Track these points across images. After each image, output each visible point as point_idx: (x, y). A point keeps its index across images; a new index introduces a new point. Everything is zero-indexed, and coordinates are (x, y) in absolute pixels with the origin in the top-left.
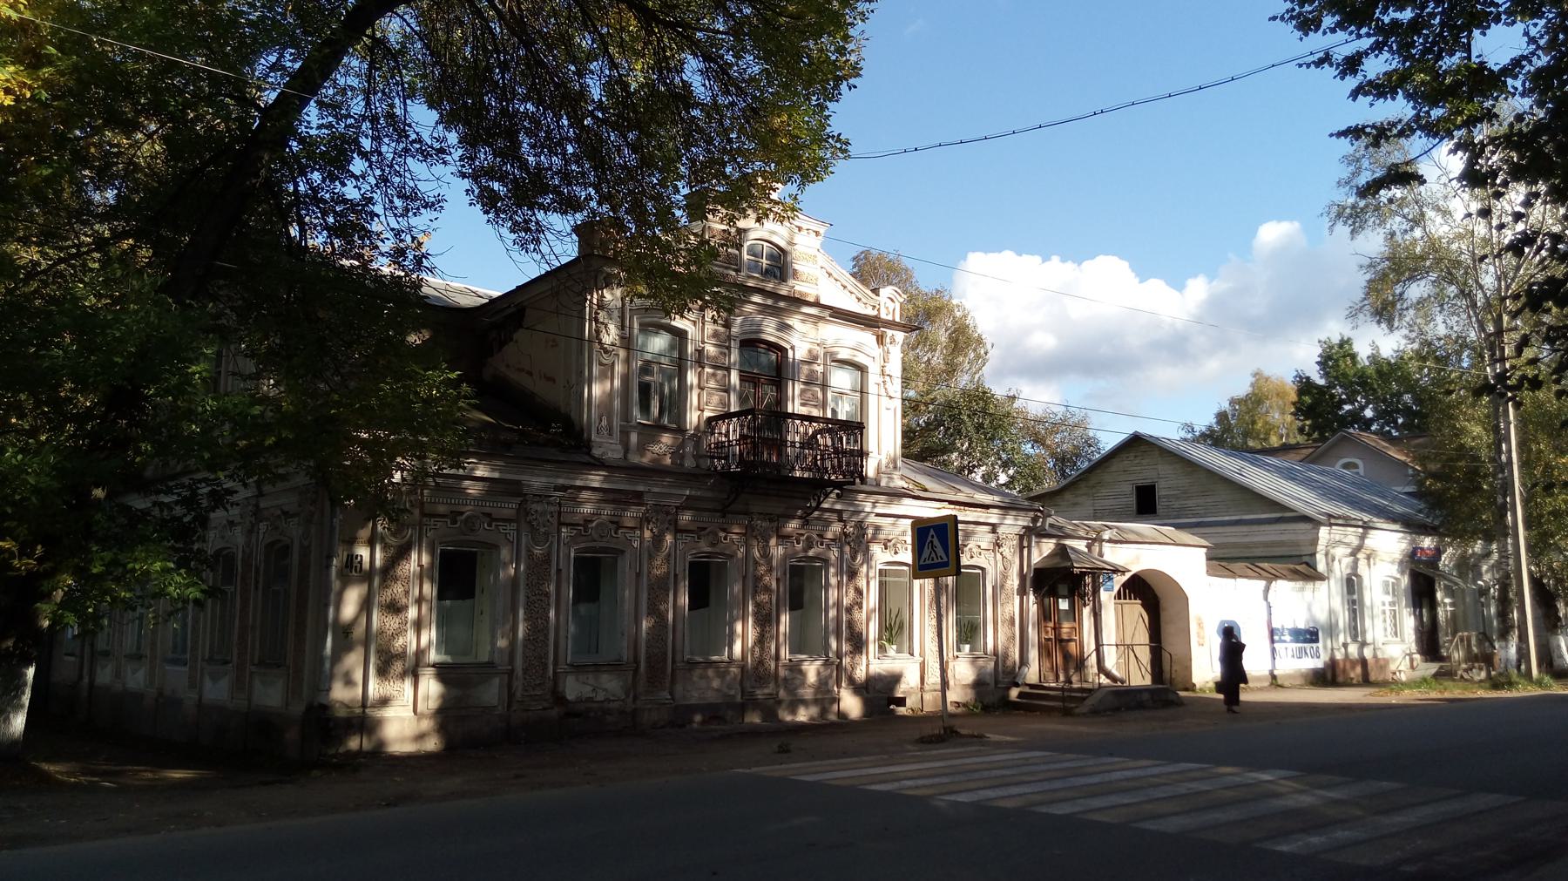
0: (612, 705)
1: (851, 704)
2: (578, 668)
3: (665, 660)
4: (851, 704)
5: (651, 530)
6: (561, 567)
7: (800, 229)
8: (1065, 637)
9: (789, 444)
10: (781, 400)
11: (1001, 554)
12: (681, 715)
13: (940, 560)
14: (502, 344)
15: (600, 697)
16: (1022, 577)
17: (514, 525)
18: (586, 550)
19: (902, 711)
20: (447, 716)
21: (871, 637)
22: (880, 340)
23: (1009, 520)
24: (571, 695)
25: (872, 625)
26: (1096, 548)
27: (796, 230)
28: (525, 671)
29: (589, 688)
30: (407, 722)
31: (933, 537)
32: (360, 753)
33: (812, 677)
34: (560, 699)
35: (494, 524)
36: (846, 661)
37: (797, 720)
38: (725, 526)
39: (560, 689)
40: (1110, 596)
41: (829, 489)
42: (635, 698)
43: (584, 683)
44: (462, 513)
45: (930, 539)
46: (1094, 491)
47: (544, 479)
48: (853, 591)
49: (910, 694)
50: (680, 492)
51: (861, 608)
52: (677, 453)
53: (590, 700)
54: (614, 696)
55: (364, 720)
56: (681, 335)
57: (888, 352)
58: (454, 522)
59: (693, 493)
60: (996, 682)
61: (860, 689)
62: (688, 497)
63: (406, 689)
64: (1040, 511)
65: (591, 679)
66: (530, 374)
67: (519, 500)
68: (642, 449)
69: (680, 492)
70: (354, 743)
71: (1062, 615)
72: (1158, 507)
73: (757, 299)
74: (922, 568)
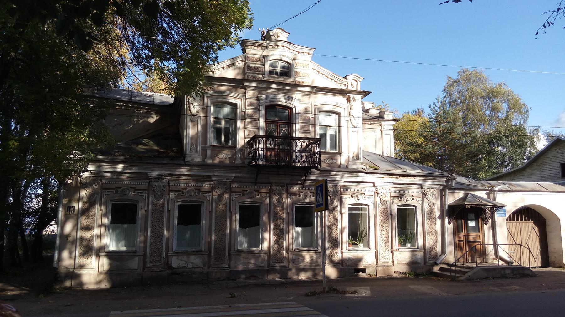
0: (196, 270)
1: (331, 272)
2: (178, 253)
3: (224, 250)
4: (331, 272)
5: (217, 192)
7: (299, 53)
8: (471, 240)
10: (290, 131)
11: (427, 198)
12: (233, 275)
15: (190, 266)
16: (442, 210)
17: (146, 192)
18: (183, 202)
19: (361, 275)
20: (110, 273)
21: (344, 240)
22: (348, 100)
23: (429, 182)
25: (344, 234)
26: (492, 195)
27: (297, 53)
28: (151, 255)
29: (184, 262)
30: (92, 275)
32: (70, 288)
33: (308, 259)
34: (170, 267)
36: (328, 252)
37: (300, 278)
38: (257, 189)
39: (169, 263)
40: (504, 220)
42: (209, 267)
44: (121, 187)
46: (541, 167)
47: (158, 172)
48: (332, 218)
49: (369, 267)
50: (230, 175)
51: (337, 226)
52: (233, 158)
54: (197, 266)
55: (73, 275)
56: (234, 106)
57: (352, 105)
58: (117, 191)
59: (237, 175)
60: (425, 262)
61: (335, 265)
62: (235, 177)
63: (93, 261)
64: (449, 177)
65: (185, 258)
67: (148, 181)
68: (213, 157)
69: (230, 175)
70: (68, 284)
71: (469, 229)
73: (273, 86)
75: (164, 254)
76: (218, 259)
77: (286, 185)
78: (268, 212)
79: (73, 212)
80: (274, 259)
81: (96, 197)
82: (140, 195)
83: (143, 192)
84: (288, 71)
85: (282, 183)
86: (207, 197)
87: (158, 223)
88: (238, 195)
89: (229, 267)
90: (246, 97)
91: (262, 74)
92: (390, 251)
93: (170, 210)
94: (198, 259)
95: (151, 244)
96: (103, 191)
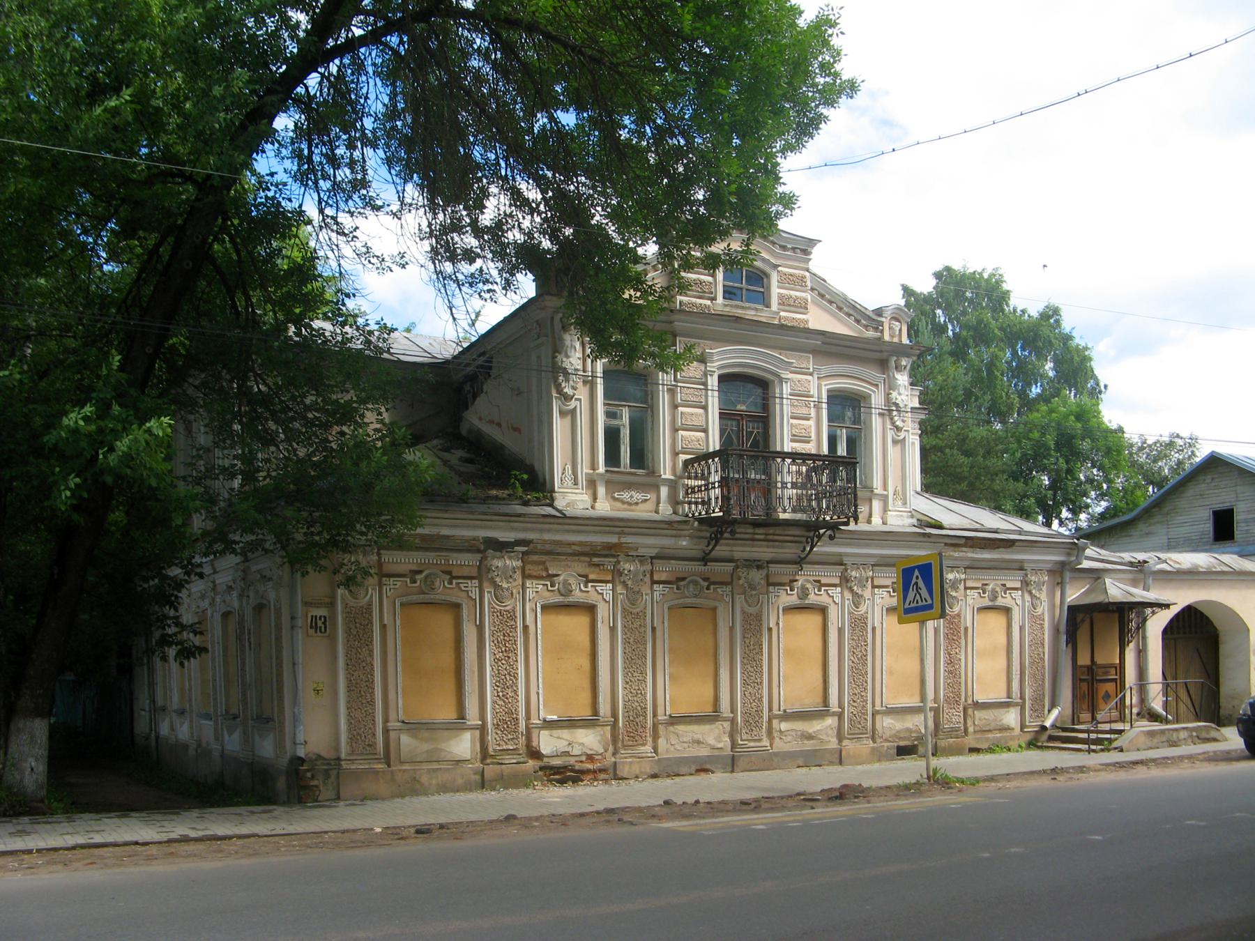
2: (549, 725)
9: (779, 485)
13: (924, 603)
14: (475, 396)
17: (476, 582)
24: (545, 750)
28: (497, 726)
31: (917, 578)
35: (454, 581)
41: (822, 531)
43: (558, 738)
45: (914, 580)
53: (566, 754)
66: (499, 425)
72: (1236, 532)
74: (907, 611)
75: (522, 724)
89: (656, 750)
92: (961, 708)
95: (494, 702)
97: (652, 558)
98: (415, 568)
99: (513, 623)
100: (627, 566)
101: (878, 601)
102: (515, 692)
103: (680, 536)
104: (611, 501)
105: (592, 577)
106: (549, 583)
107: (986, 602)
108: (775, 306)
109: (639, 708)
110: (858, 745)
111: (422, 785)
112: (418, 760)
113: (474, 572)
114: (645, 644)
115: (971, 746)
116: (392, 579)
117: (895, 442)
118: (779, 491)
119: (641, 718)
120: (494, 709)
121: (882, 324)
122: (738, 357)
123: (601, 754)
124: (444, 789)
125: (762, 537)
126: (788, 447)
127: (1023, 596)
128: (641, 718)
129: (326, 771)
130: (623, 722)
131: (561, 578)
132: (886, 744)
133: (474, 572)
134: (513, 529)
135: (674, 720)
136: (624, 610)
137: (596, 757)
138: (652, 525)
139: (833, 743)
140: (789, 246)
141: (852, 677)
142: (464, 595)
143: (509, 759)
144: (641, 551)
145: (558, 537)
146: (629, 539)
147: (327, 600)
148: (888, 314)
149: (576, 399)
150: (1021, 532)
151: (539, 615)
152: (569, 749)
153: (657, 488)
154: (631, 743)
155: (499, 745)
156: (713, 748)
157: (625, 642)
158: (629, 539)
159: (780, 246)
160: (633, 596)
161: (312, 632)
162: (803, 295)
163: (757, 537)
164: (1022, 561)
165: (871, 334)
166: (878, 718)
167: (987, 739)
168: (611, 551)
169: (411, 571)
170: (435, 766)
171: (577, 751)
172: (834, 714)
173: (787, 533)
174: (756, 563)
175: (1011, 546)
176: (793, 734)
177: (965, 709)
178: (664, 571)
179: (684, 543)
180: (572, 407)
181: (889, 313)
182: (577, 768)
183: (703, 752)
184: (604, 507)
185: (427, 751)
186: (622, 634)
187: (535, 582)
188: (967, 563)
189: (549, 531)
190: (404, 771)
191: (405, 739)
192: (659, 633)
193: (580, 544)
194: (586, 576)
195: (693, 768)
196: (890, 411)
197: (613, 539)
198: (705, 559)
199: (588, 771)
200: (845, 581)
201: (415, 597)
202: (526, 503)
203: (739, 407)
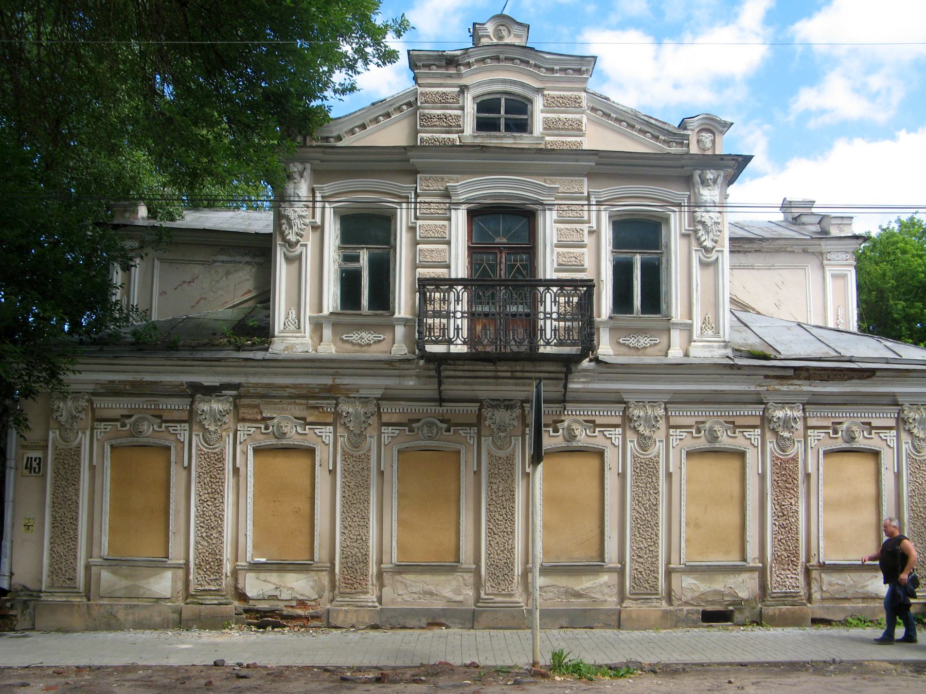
2: (256, 567)
6: (671, 471)
9: (541, 316)
17: (186, 426)
28: (199, 566)
35: (164, 425)
43: (265, 581)
53: (274, 598)
54: (302, 595)
75: (227, 567)
76: (350, 581)
77: (519, 404)
78: (330, 471)
79: (37, 470)
80: (488, 584)
81: (515, 444)
82: (172, 432)
83: (179, 426)
84: (527, 119)
85: (510, 400)
86: (886, 440)
87: (211, 496)
88: (398, 431)
89: (380, 600)
90: (418, 191)
91: (457, 132)
92: (800, 569)
93: (382, 469)
94: (305, 580)
95: (197, 543)
96: (95, 423)
97: (378, 399)
98: (126, 412)
99: (220, 465)
100: (345, 408)
101: (673, 441)
102: (220, 533)
103: (405, 376)
104: (340, 344)
105: (309, 419)
106: (263, 426)
107: (840, 444)
108: (538, 127)
109: (360, 555)
110: (644, 607)
111: (118, 620)
112: (118, 595)
113: (185, 416)
114: (368, 488)
115: (818, 616)
116: (103, 424)
117: (704, 265)
118: (541, 323)
119: (362, 564)
120: (196, 549)
121: (687, 137)
122: (489, 188)
123: (315, 600)
124: (140, 625)
125: (509, 374)
126: (551, 275)
127: (898, 437)
128: (362, 564)
129: (25, 601)
130: (340, 569)
131: (275, 421)
132: (686, 608)
133: (185, 416)
134: (217, 374)
135: (401, 569)
136: (344, 453)
137: (309, 603)
138: (309, 364)
139: (611, 602)
140: (557, 68)
141: (636, 528)
142: (173, 438)
143: (210, 600)
144: (363, 393)
145: (266, 380)
146: (346, 381)
147: (42, 443)
148: (694, 124)
149: (302, 245)
150: (900, 361)
151: (821, 461)
152: (277, 593)
153: (392, 327)
154: (348, 590)
155: (201, 585)
156: (450, 601)
157: (345, 485)
158: (346, 381)
159: (547, 69)
160: (357, 439)
161: (26, 472)
162: (577, 116)
163: (500, 374)
164: (893, 395)
165: (675, 149)
166: (674, 577)
167: (844, 609)
168: (331, 393)
169: (122, 416)
170: (135, 602)
171: (285, 595)
172: (610, 570)
173: (538, 369)
174: (506, 403)
175: (869, 377)
176: (555, 590)
177: (807, 571)
178: (392, 412)
179: (411, 383)
180: (297, 253)
181: (696, 124)
182: (285, 613)
183: (438, 605)
184: (329, 348)
185: (126, 587)
186: (342, 477)
187: (247, 424)
188: (805, 399)
189: (255, 374)
190: (101, 605)
191: (106, 575)
192: (675, 479)
193: (295, 386)
194: (304, 419)
195: (424, 622)
196: (696, 232)
197: (328, 381)
198: (441, 400)
199: (298, 617)
200: (627, 421)
201: (124, 440)
202: (238, 349)
203: (498, 240)
